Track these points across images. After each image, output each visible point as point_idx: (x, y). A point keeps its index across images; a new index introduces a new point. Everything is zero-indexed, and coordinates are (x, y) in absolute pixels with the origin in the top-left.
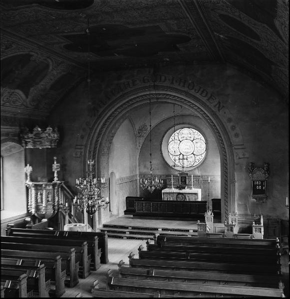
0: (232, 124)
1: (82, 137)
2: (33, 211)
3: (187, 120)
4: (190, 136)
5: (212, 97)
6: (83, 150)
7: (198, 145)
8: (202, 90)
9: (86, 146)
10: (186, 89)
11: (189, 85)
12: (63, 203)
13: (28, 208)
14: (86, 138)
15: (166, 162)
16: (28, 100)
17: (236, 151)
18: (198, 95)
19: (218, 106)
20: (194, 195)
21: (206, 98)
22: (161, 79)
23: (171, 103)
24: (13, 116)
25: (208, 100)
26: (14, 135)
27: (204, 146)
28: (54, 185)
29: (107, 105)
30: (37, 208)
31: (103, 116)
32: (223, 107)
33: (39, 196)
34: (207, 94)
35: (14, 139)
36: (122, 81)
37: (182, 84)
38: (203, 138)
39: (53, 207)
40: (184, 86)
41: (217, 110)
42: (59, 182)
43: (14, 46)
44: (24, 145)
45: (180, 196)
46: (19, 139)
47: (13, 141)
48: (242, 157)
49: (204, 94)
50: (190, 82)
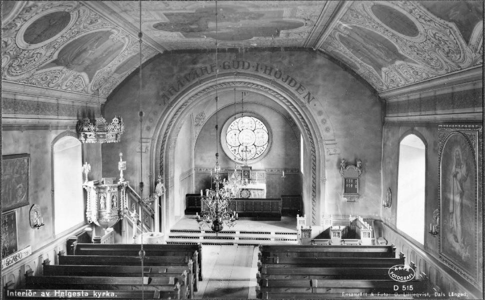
0: (322, 117)
1: (149, 129)
2: (93, 218)
3: (249, 108)
4: (251, 125)
5: (302, 87)
6: (149, 144)
7: (260, 135)
8: (290, 79)
9: (153, 139)
10: (272, 78)
11: (276, 73)
12: (127, 207)
13: (85, 215)
14: (153, 130)
15: (226, 155)
16: (91, 84)
17: (327, 146)
18: (286, 85)
19: (307, 97)
20: (260, 191)
21: (294, 89)
22: (243, 65)
23: (253, 92)
24: (71, 103)
25: (297, 90)
26: (72, 127)
27: (266, 137)
28: (119, 187)
29: (179, 93)
30: (99, 216)
31: (174, 105)
32: (313, 98)
33: (102, 201)
34: (296, 84)
35: (72, 132)
36: (198, 66)
37: (268, 72)
38: (265, 128)
39: (119, 213)
40: (270, 74)
41: (307, 102)
42: (125, 183)
43: (100, 21)
44: (83, 139)
45: (244, 192)
46: (78, 130)
47: (71, 134)
48: (334, 153)
49: (292, 84)
50: (277, 70)
